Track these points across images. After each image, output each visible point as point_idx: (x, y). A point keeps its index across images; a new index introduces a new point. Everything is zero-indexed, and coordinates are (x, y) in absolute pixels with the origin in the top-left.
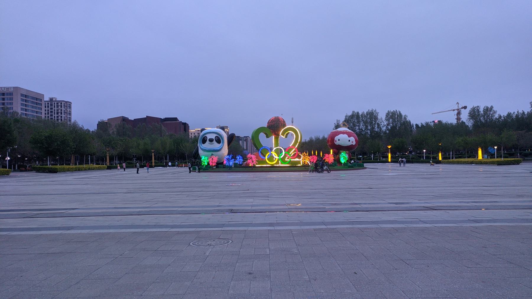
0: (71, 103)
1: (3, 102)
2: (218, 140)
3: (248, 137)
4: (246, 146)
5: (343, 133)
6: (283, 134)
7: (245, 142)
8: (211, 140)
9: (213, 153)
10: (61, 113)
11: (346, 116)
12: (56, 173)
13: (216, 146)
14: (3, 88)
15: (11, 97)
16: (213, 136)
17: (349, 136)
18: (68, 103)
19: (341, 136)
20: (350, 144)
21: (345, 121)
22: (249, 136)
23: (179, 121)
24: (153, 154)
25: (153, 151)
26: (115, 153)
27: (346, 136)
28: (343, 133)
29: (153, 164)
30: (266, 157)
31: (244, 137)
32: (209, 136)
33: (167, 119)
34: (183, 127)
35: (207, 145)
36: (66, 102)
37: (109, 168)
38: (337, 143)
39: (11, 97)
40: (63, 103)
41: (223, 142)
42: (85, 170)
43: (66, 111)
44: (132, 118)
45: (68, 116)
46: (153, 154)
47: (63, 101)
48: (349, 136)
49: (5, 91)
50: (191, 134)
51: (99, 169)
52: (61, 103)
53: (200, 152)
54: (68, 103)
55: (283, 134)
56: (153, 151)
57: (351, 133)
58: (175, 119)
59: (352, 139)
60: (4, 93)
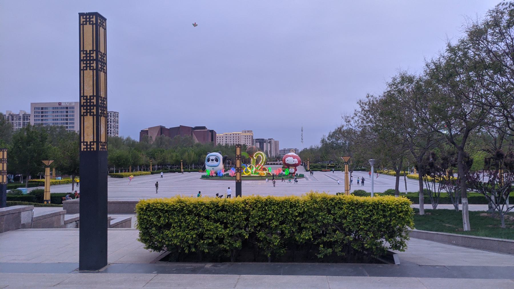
0: (118, 113)
1: (67, 114)
2: (217, 160)
3: (272, 139)
4: (270, 147)
5: (290, 156)
6: (255, 156)
7: (269, 144)
8: (212, 160)
9: (214, 168)
10: (111, 122)
11: (330, 133)
12: (122, 178)
13: (215, 163)
14: (67, 103)
15: (73, 110)
16: (214, 158)
17: (294, 159)
18: (116, 113)
19: (289, 158)
20: (294, 163)
21: (329, 136)
22: (273, 139)
23: (207, 129)
24: (182, 163)
25: (182, 161)
26: (155, 162)
27: (292, 158)
28: (290, 156)
29: (182, 170)
30: (244, 171)
31: (269, 139)
32: (211, 158)
33: (197, 128)
34: (210, 134)
35: (210, 163)
36: (115, 112)
37: (152, 173)
38: (287, 162)
39: (73, 110)
40: (112, 113)
41: (220, 161)
42: (138, 175)
43: (114, 120)
44: (168, 127)
45: (116, 124)
46: (182, 163)
47: (112, 112)
48: (294, 159)
49: (68, 105)
50: (218, 137)
51: (146, 174)
52: (111, 114)
53: (206, 167)
54: (116, 113)
55: (255, 156)
56: (182, 161)
57: (296, 156)
58: (204, 128)
59: (296, 160)
60: (68, 107)
